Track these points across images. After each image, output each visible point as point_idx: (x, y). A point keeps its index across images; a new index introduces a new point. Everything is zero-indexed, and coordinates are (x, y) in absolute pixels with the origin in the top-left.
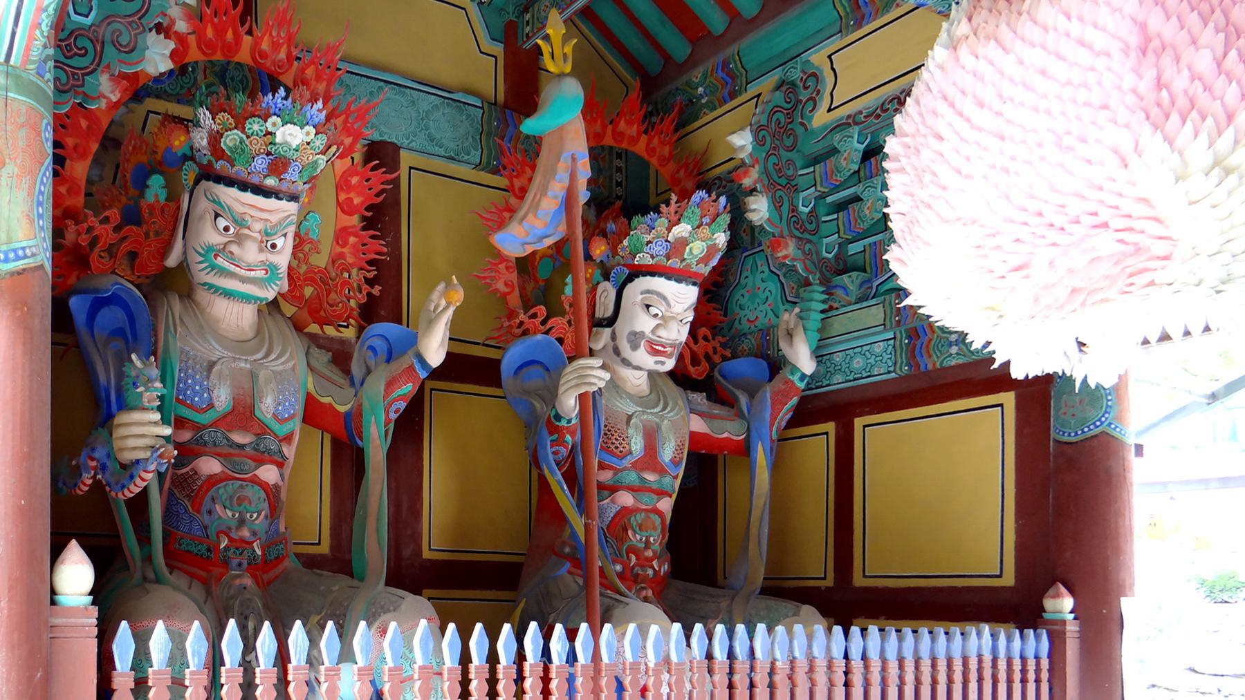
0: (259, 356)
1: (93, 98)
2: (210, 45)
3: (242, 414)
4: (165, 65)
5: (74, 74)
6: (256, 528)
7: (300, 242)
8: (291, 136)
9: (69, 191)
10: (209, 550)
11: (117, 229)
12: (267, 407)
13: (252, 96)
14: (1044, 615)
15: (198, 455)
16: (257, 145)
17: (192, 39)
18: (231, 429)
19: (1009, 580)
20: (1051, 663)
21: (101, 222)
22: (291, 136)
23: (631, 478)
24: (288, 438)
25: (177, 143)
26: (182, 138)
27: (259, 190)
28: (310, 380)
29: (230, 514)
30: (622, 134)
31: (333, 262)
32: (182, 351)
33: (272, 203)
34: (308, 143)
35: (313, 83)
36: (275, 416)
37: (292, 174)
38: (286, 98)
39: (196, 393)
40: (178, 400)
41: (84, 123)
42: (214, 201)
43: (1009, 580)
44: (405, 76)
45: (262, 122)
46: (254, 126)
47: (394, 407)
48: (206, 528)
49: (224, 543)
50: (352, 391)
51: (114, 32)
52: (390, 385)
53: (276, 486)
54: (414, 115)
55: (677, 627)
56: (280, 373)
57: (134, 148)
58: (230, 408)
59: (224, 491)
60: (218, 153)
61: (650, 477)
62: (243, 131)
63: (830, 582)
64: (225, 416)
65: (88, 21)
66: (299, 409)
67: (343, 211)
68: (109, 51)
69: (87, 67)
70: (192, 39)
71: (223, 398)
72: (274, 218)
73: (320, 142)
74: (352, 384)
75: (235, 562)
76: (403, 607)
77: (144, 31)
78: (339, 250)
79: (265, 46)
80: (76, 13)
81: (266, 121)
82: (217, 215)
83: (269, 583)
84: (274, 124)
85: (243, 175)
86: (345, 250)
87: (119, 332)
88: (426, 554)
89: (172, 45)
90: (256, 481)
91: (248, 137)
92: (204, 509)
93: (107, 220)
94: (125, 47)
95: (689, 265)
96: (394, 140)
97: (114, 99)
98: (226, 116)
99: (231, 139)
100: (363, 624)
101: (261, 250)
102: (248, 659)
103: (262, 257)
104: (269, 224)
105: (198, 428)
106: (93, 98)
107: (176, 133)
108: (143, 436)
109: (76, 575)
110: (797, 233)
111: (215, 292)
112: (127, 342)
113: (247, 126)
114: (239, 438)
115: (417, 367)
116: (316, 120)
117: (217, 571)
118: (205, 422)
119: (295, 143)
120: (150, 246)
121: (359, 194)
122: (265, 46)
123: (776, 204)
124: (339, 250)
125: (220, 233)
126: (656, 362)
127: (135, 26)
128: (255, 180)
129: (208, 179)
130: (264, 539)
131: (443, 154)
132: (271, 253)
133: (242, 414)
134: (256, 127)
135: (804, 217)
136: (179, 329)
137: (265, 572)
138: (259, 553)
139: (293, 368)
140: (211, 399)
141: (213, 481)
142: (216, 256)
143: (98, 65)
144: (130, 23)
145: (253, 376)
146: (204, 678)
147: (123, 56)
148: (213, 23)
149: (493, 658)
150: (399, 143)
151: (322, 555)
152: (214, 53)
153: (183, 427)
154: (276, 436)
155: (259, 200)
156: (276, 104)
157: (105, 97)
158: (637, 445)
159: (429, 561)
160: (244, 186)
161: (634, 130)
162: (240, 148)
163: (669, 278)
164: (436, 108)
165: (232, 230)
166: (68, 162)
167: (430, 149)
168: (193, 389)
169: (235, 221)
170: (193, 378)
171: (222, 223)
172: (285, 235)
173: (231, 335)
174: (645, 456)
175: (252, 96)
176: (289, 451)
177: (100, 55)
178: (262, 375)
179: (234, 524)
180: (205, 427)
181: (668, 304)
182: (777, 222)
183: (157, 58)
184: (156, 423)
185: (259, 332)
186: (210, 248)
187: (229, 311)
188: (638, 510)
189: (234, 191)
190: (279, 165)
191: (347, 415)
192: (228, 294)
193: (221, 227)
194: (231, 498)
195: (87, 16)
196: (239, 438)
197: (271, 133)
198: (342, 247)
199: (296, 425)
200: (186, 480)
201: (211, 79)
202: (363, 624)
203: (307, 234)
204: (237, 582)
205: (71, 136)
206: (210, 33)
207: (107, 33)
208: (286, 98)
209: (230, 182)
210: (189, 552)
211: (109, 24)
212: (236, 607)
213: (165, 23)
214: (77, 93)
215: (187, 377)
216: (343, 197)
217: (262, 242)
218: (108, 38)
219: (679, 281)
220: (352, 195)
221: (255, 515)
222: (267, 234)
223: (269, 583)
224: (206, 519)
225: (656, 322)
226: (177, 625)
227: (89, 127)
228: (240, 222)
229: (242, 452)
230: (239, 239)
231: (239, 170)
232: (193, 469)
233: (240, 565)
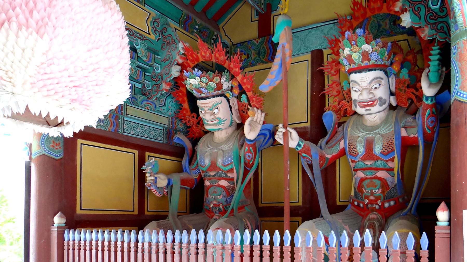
0: (379, 130)
2: (204, 57)
12: (219, 162)
14: (437, 222)
19: (300, 204)
20: (64, 243)
23: (361, 165)
24: (231, 170)
30: (374, 9)
33: (208, 101)
35: (219, 58)
36: (223, 165)
41: (180, 94)
43: (300, 204)
55: (237, 232)
58: (210, 165)
59: (365, 183)
61: (369, 163)
63: (136, 213)
65: (433, 7)
72: (211, 105)
79: (203, 54)
88: (79, 211)
90: (219, 186)
95: (359, 64)
107: (398, 65)
109: (58, 220)
110: (433, 21)
114: (212, 173)
121: (248, 84)
122: (203, 54)
123: (416, 13)
126: (366, 110)
130: (225, 204)
135: (437, 11)
136: (350, 128)
149: (261, 243)
151: (299, 206)
158: (361, 149)
161: (379, 4)
163: (356, 73)
164: (331, 28)
174: (366, 154)
181: (358, 84)
182: (418, 21)
188: (366, 179)
201: (256, 56)
219: (360, 72)
221: (218, 197)
225: (374, 91)
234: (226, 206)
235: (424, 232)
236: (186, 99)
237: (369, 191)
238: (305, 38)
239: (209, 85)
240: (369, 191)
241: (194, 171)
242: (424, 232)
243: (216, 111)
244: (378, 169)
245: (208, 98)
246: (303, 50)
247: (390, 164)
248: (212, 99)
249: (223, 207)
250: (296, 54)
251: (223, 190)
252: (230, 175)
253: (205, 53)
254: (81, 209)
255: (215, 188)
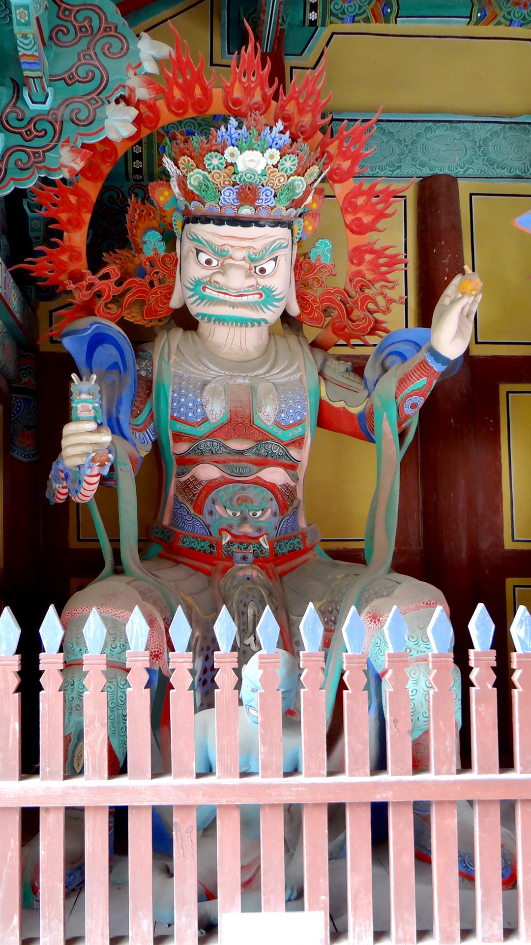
0: (261, 372)
1: (55, 170)
2: (181, 105)
3: (240, 423)
4: (128, 130)
5: (34, 153)
6: (261, 524)
7: (303, 269)
8: (252, 162)
9: (71, 258)
10: (211, 546)
11: (119, 283)
12: (267, 415)
13: (207, 134)
15: (195, 463)
16: (219, 178)
17: (161, 104)
18: (229, 437)
21: (101, 278)
22: (252, 162)
24: (298, 442)
25: (162, 199)
26: (166, 193)
27: (235, 221)
28: (323, 388)
29: (230, 513)
31: (351, 281)
32: (176, 375)
33: (253, 231)
34: (276, 166)
35: (296, 118)
36: (277, 424)
37: (265, 199)
38: (239, 127)
39: (189, 409)
40: (173, 418)
41: (73, 199)
42: (194, 240)
44: (462, 113)
45: (219, 155)
46: (213, 160)
47: (409, 402)
48: (208, 527)
49: (226, 539)
50: (366, 393)
51: (73, 111)
52: (403, 382)
53: (286, 486)
54: (469, 145)
56: (283, 384)
57: (140, 216)
58: (225, 420)
59: (221, 494)
60: (190, 196)
62: (204, 169)
64: (221, 427)
65: (46, 107)
66: (310, 415)
67: (352, 231)
68: (69, 128)
69: (48, 145)
70: (161, 104)
71: (217, 411)
72: (258, 245)
73: (290, 163)
74: (366, 387)
75: (238, 556)
76: (396, 592)
77: (103, 103)
78: (355, 268)
80: (33, 102)
81: (223, 154)
82: (198, 252)
83: (282, 575)
84: (232, 155)
85: (217, 211)
86: (363, 268)
87: (115, 366)
88: (508, 545)
89: (133, 112)
91: (210, 172)
92: (206, 510)
93: (106, 276)
94: (84, 121)
96: (447, 172)
97: (78, 168)
98: (186, 158)
99: (195, 178)
100: (353, 608)
101: (248, 276)
102: (247, 642)
103: (252, 281)
104: (251, 250)
105: (192, 439)
106: (55, 170)
108: (81, 444)
111: (209, 321)
112: (120, 372)
113: (206, 162)
114: (236, 445)
115: (430, 361)
116: (281, 143)
117: (221, 564)
118: (201, 434)
119: (259, 169)
120: (156, 293)
121: (368, 212)
124: (355, 268)
125: (204, 268)
127: (93, 102)
128: (229, 212)
129: (188, 223)
130: (273, 533)
131: (507, 174)
132: (262, 277)
133: (240, 423)
134: (215, 162)
136: (173, 357)
137: (277, 565)
138: (267, 547)
139: (301, 380)
140: (205, 413)
141: (212, 486)
142: (204, 288)
143: (58, 141)
144: (89, 101)
145: (252, 389)
146: (491, 658)
147: (82, 130)
148: (178, 85)
150: (453, 174)
152: (184, 113)
153: (181, 440)
154: (279, 441)
155: (239, 231)
156: (230, 135)
157: (65, 167)
159: (514, 552)
160: (220, 221)
162: (204, 185)
165: (215, 263)
166: (65, 234)
167: (491, 172)
168: (187, 406)
169: (215, 253)
170: (186, 397)
171: (203, 257)
172: (275, 259)
173: (235, 357)
175: (207, 134)
176: (302, 455)
177: (58, 134)
178: (262, 387)
179: (235, 522)
180: (201, 438)
183: (116, 124)
184: (91, 432)
185: (265, 352)
186: (198, 282)
187: (231, 336)
189: (211, 227)
190: (248, 193)
191: (361, 415)
192: (221, 320)
193: (203, 261)
194: (231, 499)
195: (44, 103)
196: (236, 445)
197: (232, 164)
198: (359, 264)
199: (308, 430)
200: (187, 486)
202: (353, 608)
203: (318, 260)
204: (241, 574)
205: (63, 212)
206: (177, 94)
207: (65, 113)
208: (239, 127)
209: (206, 220)
210: (192, 548)
211: (67, 106)
212: (236, 596)
213: (126, 93)
214: (40, 168)
215: (180, 396)
216: (349, 218)
217: (250, 269)
218: (67, 117)
220: (359, 215)
221: (259, 513)
222: (252, 260)
223: (282, 575)
224: (208, 519)
226: (110, 612)
227: (78, 201)
228: (221, 253)
229: (242, 458)
230: (223, 270)
231: (210, 207)
232: (193, 476)
233: (244, 558)
234: (279, 541)
235: (481, 607)
236: (87, 217)
237: (238, 514)
238: (414, 142)
239: (293, 181)
240: (238, 514)
241: (141, 434)
242: (481, 607)
243: (269, 266)
244: (262, 464)
245: (258, 223)
246: (407, 170)
247: (294, 453)
248: (267, 230)
249: (271, 544)
250: (381, 173)
251: (271, 495)
252: (294, 453)
253: (249, 91)
254: (513, 540)
255: (243, 489)
